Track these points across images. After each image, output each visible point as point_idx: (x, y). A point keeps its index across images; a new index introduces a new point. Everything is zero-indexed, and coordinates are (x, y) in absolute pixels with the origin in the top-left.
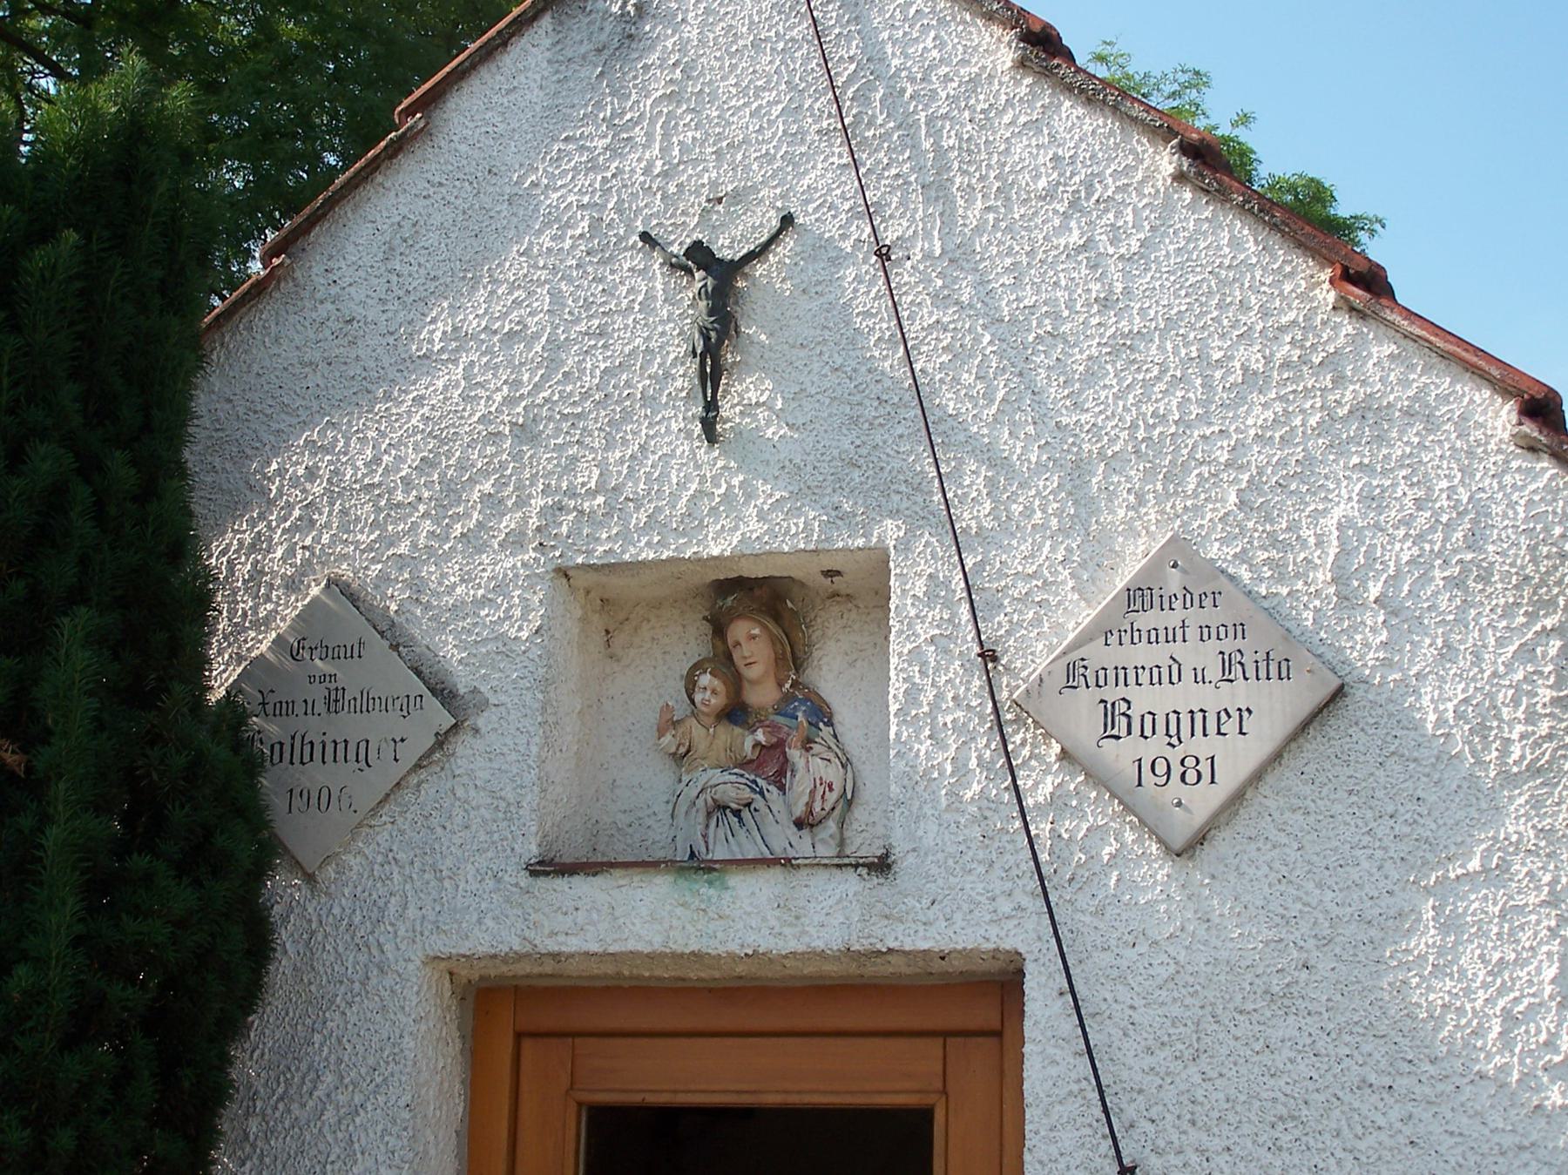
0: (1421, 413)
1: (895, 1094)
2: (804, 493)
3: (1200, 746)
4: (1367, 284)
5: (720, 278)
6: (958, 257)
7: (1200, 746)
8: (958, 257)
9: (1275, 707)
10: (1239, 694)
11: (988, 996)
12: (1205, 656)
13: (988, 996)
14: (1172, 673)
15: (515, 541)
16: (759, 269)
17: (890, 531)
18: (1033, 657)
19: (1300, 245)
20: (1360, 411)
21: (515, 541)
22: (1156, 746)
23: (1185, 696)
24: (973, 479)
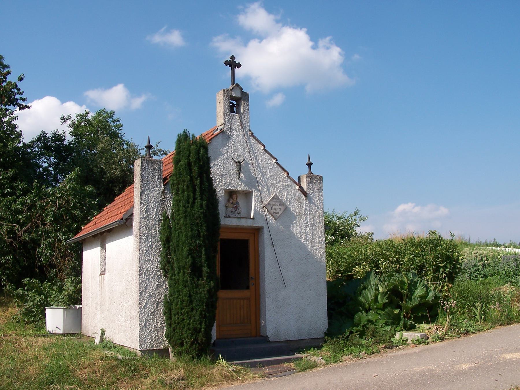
0: (291, 186)
1: (246, 238)
2: (246, 185)
3: (278, 211)
4: (102, 273)
5: (239, 163)
6: (258, 166)
7: (278, 211)
8: (258, 166)
9: (283, 208)
10: (280, 207)
11: (257, 231)
12: (278, 204)
13: (257, 231)
14: (275, 205)
15: (222, 186)
16: (107, 334)
17: (253, 190)
18: (265, 203)
19: (167, 241)
20: (288, 185)
21: (222, 186)
22: (274, 211)
23: (277, 207)
24: (260, 186)
